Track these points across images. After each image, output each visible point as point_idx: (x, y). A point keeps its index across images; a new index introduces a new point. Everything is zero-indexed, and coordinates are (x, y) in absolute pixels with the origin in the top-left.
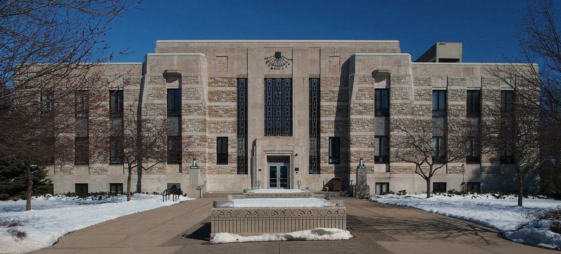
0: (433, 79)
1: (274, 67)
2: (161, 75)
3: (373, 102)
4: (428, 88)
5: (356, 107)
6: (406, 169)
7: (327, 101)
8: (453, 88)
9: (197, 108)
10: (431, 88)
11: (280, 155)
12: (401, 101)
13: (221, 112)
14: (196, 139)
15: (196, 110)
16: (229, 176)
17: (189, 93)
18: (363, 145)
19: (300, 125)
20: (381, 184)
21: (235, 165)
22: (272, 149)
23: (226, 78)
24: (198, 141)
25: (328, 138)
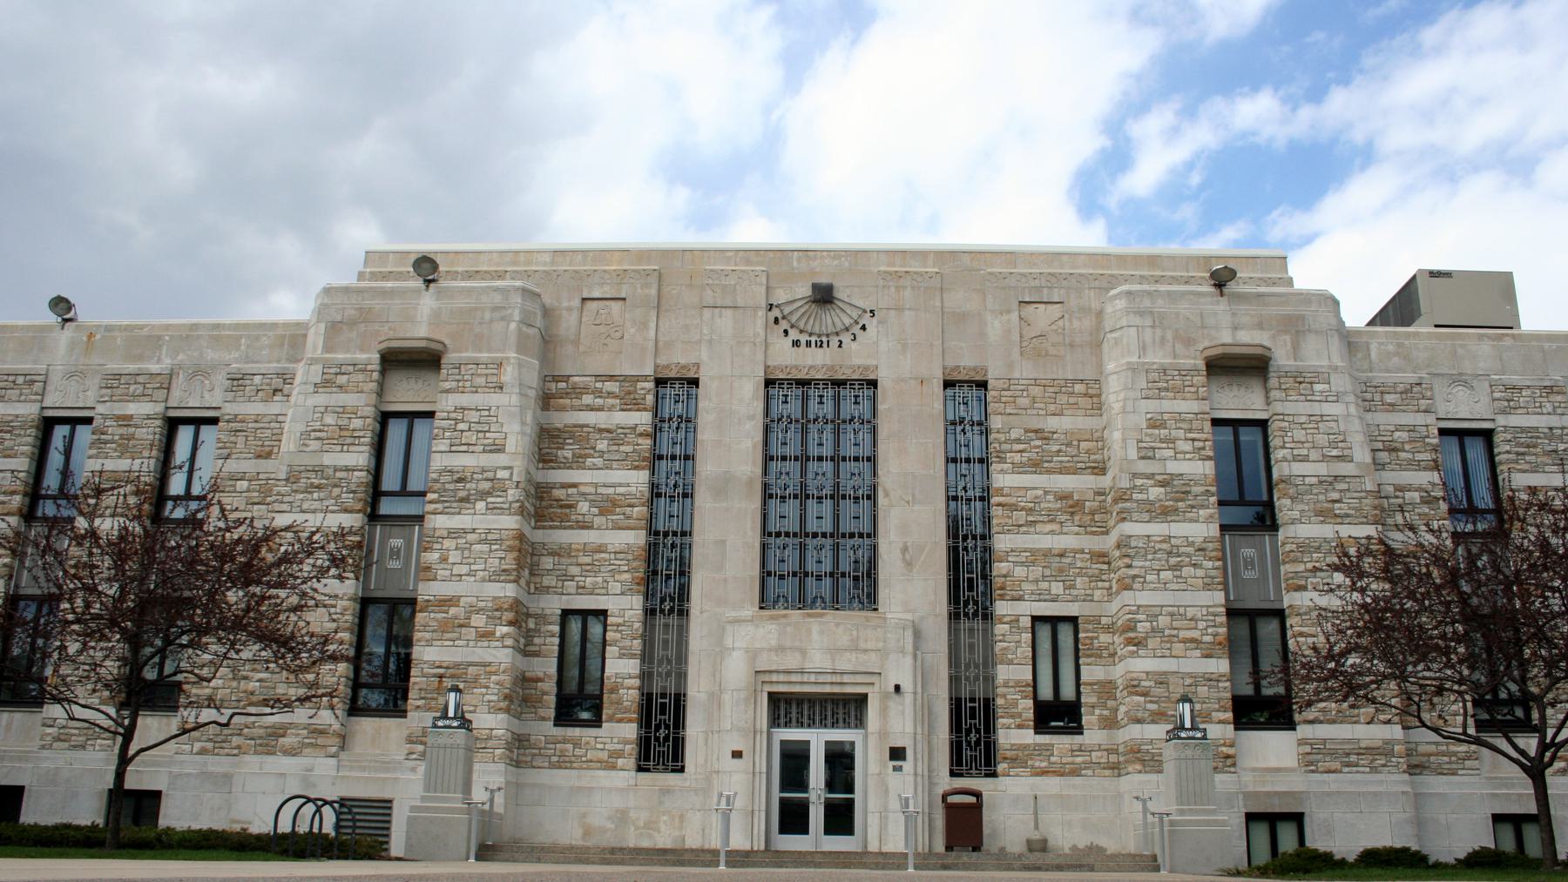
0: (1440, 389)
1: (803, 338)
2: (1201, 365)
3: (1208, 468)
4: (1420, 419)
5: (1142, 489)
6: (1370, 750)
7: (1018, 468)
8: (1516, 420)
9: (486, 486)
10: (1430, 419)
11: (828, 689)
12: (1322, 469)
13: (583, 507)
14: (474, 610)
15: (483, 495)
16: (604, 778)
17: (461, 426)
18: (1178, 648)
19: (909, 564)
20: (1272, 820)
21: (630, 731)
22: (792, 661)
23: (612, 378)
24: (479, 621)
25: (1026, 622)
